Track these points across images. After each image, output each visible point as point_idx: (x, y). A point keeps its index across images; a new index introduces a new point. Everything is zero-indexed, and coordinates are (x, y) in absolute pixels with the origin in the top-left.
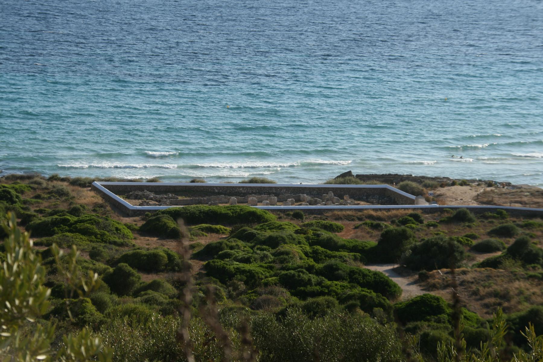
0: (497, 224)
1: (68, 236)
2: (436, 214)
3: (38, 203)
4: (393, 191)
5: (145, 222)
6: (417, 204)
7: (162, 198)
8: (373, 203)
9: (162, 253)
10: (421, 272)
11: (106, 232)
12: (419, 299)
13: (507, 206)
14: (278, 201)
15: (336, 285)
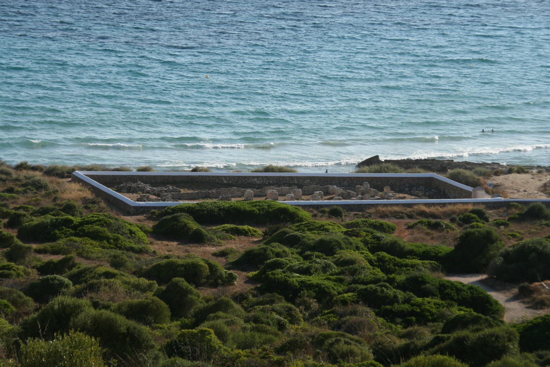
1: (76, 242)
2: (501, 210)
3: (14, 198)
4: (442, 181)
5: (157, 222)
6: (476, 198)
7: (161, 191)
9: (202, 263)
10: (522, 285)
11: (119, 236)
12: (540, 320)
14: (303, 194)
15: (429, 303)
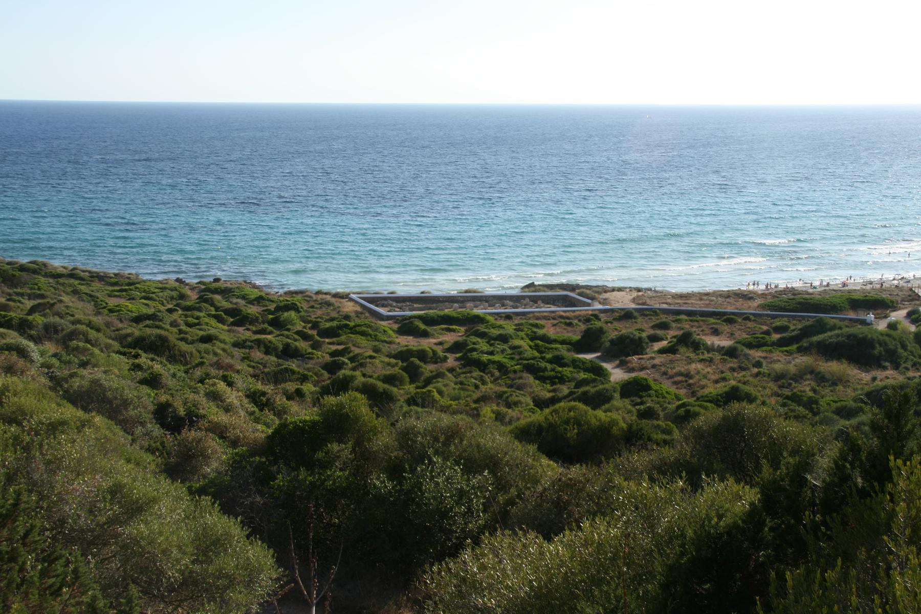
0: (655, 320)
8: (559, 306)
13: (657, 306)
